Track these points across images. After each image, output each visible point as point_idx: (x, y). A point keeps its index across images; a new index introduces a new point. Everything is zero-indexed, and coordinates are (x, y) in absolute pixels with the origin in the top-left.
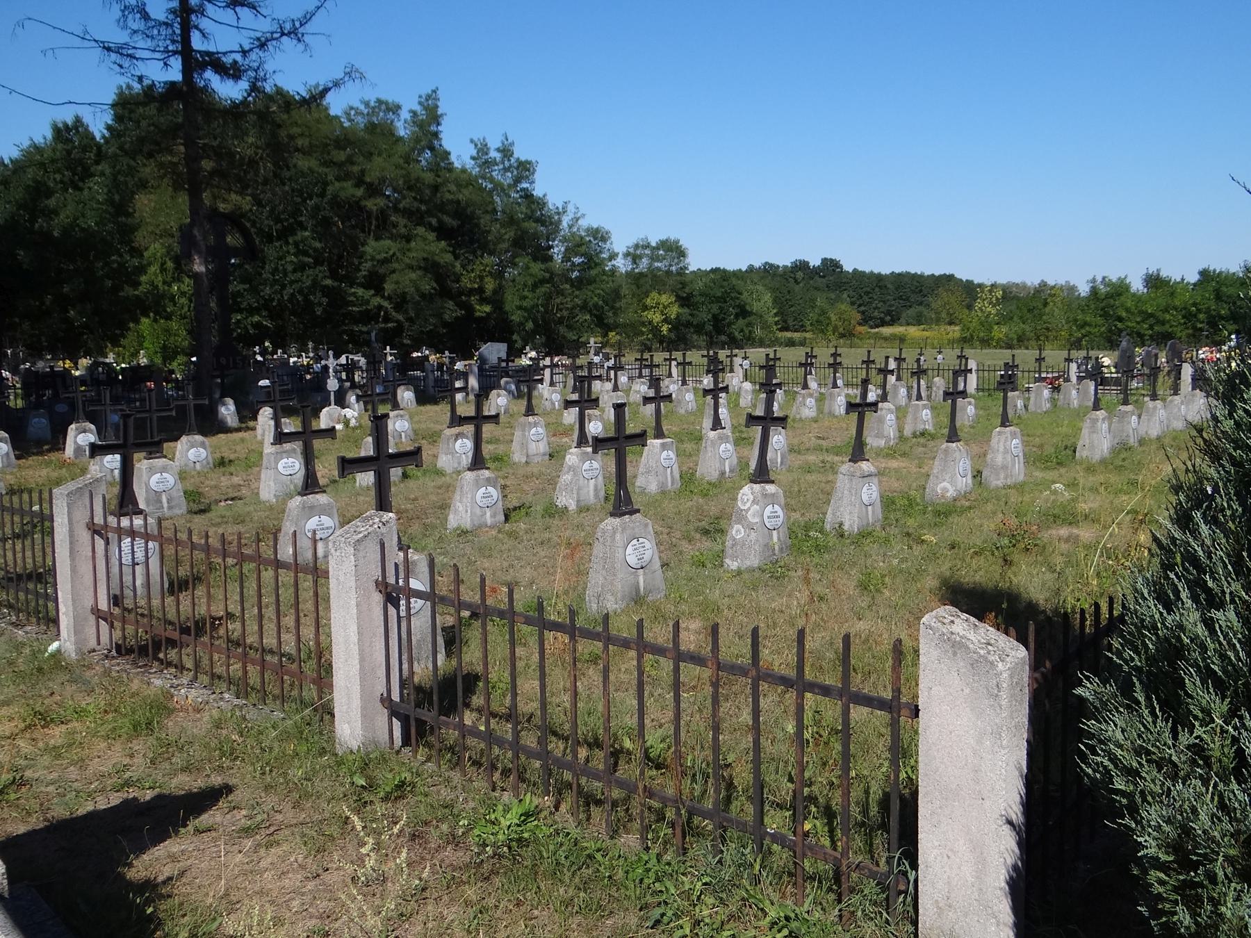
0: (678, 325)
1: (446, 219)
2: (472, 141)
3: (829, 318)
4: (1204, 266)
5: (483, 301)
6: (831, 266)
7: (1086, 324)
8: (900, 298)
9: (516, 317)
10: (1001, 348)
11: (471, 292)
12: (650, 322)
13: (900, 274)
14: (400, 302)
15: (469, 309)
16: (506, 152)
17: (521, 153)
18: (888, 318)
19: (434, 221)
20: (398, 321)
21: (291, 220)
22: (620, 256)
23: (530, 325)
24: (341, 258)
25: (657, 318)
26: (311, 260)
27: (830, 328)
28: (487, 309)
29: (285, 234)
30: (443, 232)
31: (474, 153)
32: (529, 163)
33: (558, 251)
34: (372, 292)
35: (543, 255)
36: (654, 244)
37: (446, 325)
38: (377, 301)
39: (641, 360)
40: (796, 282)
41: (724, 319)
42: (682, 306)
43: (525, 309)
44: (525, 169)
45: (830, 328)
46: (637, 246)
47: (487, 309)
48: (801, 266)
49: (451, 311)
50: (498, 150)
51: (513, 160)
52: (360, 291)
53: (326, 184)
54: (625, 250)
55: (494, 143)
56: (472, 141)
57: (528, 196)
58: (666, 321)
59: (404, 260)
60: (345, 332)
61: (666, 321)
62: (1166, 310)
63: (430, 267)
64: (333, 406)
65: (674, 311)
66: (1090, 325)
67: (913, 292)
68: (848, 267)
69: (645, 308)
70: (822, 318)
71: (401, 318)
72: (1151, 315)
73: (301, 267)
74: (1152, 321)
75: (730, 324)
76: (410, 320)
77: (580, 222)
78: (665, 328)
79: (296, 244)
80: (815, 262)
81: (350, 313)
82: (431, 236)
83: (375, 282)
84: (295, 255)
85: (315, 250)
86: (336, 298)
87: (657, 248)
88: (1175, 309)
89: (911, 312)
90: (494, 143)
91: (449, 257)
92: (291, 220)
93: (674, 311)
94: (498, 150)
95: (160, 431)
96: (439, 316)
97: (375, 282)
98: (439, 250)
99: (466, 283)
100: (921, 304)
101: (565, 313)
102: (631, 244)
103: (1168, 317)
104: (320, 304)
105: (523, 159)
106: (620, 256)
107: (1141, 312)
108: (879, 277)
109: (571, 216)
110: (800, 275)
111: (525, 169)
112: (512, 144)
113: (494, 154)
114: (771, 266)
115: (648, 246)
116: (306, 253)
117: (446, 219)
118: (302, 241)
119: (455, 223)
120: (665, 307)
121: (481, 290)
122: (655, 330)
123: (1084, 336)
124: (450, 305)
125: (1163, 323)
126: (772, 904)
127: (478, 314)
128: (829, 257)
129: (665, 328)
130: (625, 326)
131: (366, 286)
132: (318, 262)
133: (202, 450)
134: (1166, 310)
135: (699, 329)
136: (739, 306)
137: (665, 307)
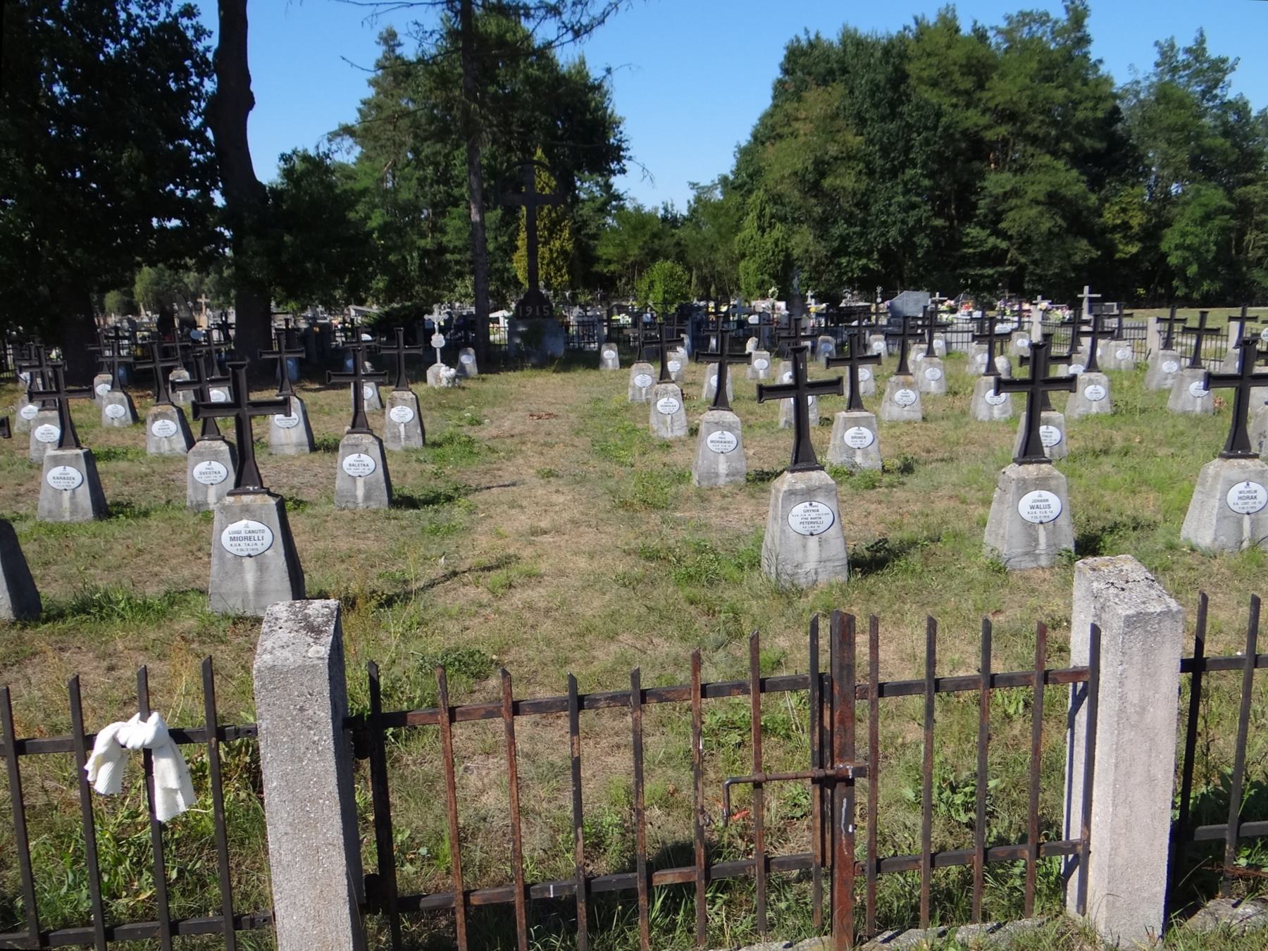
1: (1088, 143)
5: (1129, 239)
11: (1115, 228)
14: (1025, 243)
15: (1110, 249)
17: (1213, 52)
19: (1067, 146)
23: (1193, 270)
24: (959, 200)
29: (894, 173)
30: (1079, 159)
31: (1157, 58)
43: (1188, 248)
44: (1217, 70)
47: (1134, 249)
49: (1083, 250)
50: (1188, 51)
53: (939, 115)
55: (1185, 40)
56: (1157, 44)
59: (1026, 190)
60: (961, 276)
63: (1054, 200)
64: (439, 363)
81: (964, 256)
83: (993, 222)
84: (904, 194)
95: (67, 383)
97: (993, 222)
98: (1071, 181)
99: (1110, 216)
111: (1217, 70)
119: (1100, 146)
121: (1126, 226)
123: (1192, 233)
124: (1084, 243)
133: (120, 407)
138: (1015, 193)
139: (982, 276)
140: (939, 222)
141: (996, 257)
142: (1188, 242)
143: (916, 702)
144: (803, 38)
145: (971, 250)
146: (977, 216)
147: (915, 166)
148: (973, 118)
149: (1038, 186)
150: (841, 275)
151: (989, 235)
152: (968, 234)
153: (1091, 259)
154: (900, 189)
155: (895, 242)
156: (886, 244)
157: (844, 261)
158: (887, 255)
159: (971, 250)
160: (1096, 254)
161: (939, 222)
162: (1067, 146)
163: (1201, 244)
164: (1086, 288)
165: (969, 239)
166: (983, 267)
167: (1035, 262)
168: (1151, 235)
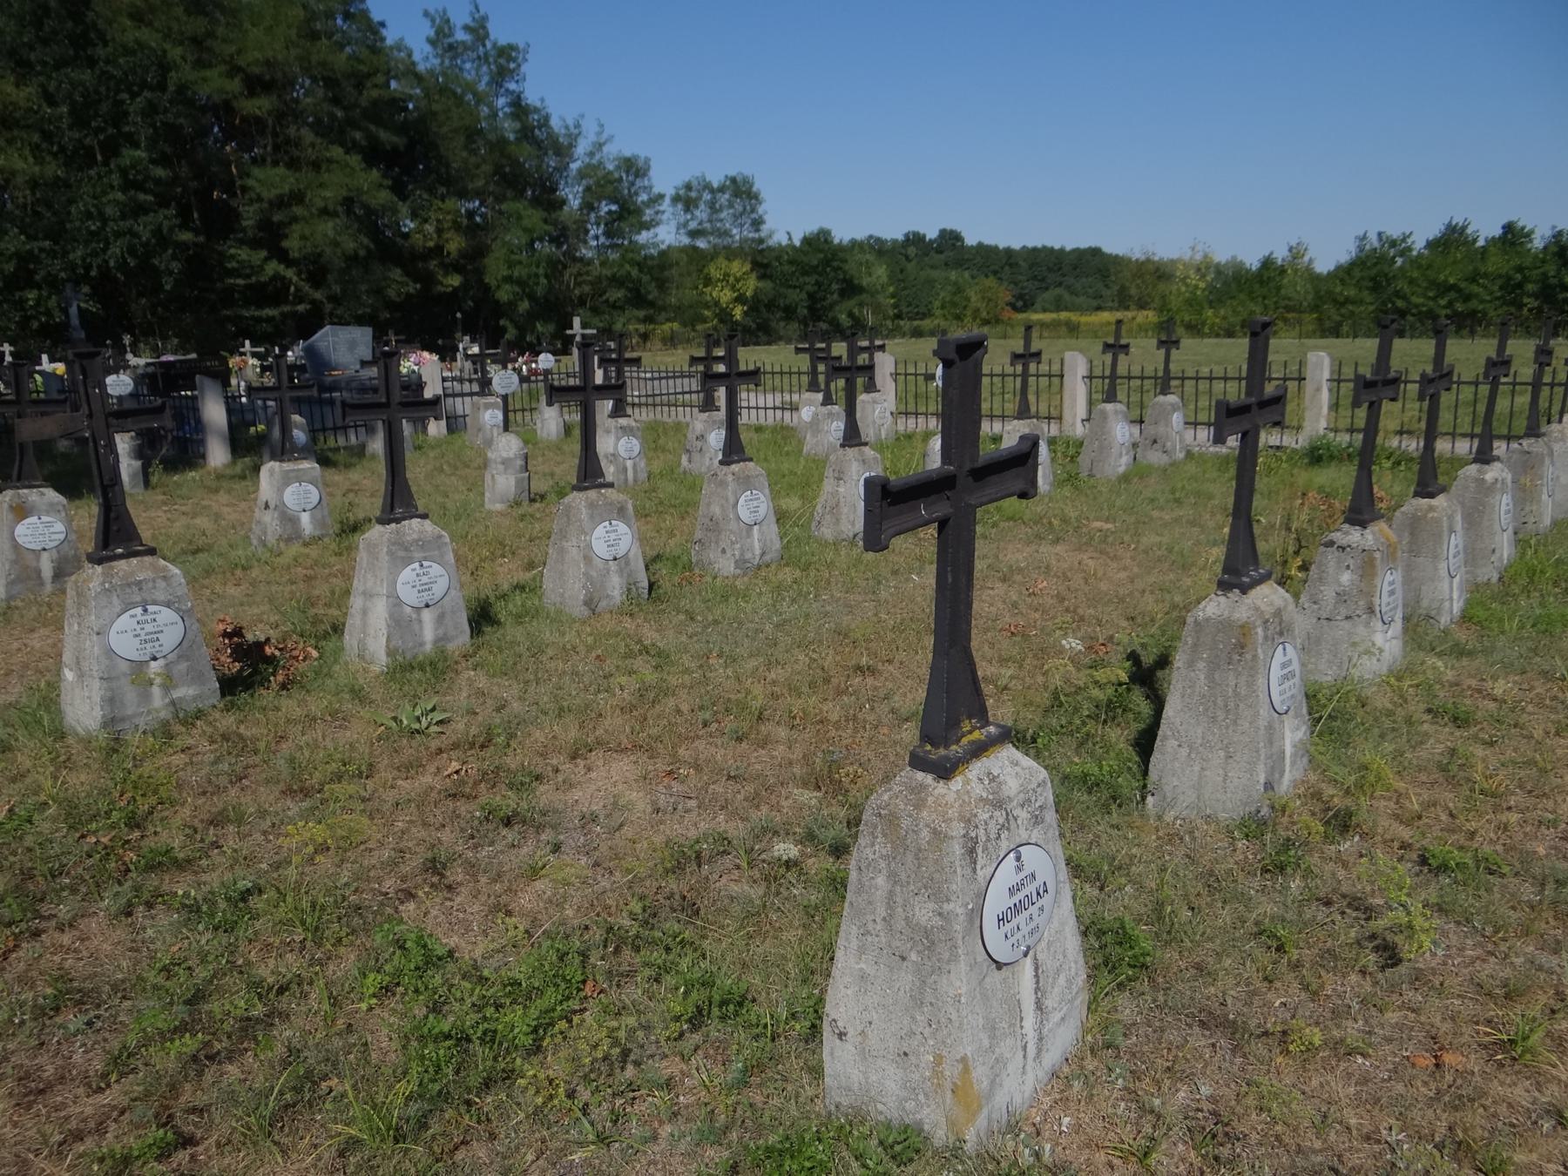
0: (754, 305)
1: (384, 135)
2: (426, 14)
3: (968, 299)
4: (1458, 220)
6: (950, 239)
7: (1347, 301)
8: (1035, 278)
9: (504, 294)
10: (1218, 336)
12: (717, 303)
13: (1035, 249)
15: (428, 280)
16: (479, 30)
17: (500, 34)
18: (1020, 304)
20: (313, 302)
21: (110, 131)
22: (667, 200)
25: (726, 296)
26: (150, 198)
27: (969, 313)
28: (455, 281)
30: (374, 155)
31: (432, 33)
32: (512, 47)
33: (573, 196)
34: (264, 254)
35: (548, 200)
36: (715, 185)
37: (390, 305)
38: (273, 267)
39: (709, 360)
40: (907, 258)
41: (824, 299)
42: (762, 277)
43: (520, 282)
44: (505, 62)
45: (969, 313)
46: (688, 187)
47: (455, 281)
48: (915, 239)
50: (466, 28)
51: (489, 45)
52: (244, 254)
54: (673, 192)
55: (460, 17)
56: (426, 14)
57: (519, 108)
58: (740, 299)
61: (740, 299)
62: (1473, 279)
65: (751, 285)
66: (1353, 303)
67: (1050, 270)
68: (970, 240)
69: (708, 281)
70: (956, 299)
71: (318, 295)
72: (1453, 287)
73: (139, 210)
74: (1453, 295)
75: (832, 306)
76: (332, 299)
77: (605, 149)
78: (738, 312)
79: (124, 172)
80: (932, 234)
82: (355, 160)
83: (270, 237)
85: (158, 181)
86: (201, 266)
87: (722, 189)
88: (1486, 276)
89: (1048, 295)
90: (460, 17)
91: (384, 196)
92: (110, 131)
93: (751, 285)
94: (466, 28)
96: (378, 292)
98: (370, 183)
100: (1060, 284)
101: (587, 289)
102: (680, 183)
103: (1475, 289)
104: (171, 273)
105: (503, 41)
106: (667, 200)
107: (1433, 283)
108: (1009, 252)
109: (592, 138)
110: (912, 251)
112: (484, 19)
113: (461, 36)
114: (878, 240)
115: (707, 186)
116: (138, 186)
117: (384, 135)
118: (133, 166)
119: (399, 141)
120: (738, 280)
122: (724, 316)
124: (396, 274)
125: (1467, 298)
126: (872, 671)
127: (440, 289)
128: (949, 227)
129: (738, 312)
130: (679, 309)
131: (255, 244)
132: (163, 202)
134: (1473, 279)
135: (789, 313)
136: (844, 280)
137: (738, 280)
138: (297, 197)
139: (259, 320)
140: (186, 236)
141: (274, 292)
142: (516, 274)
143: (1459, 431)
144: (1373, 237)
145: (240, 282)
146: (244, 230)
147: (136, 146)
148: (214, 84)
149: (330, 192)
150: (26, 320)
151: (266, 259)
152: (233, 257)
153: (408, 295)
154: (116, 179)
155: (123, 265)
156: (105, 272)
157: (31, 295)
158: (104, 286)
159: (240, 282)
160: (413, 288)
161: (186, 236)
162: (358, 135)
163: (529, 277)
164: (247, 342)
165: (234, 264)
166: (260, 306)
167: (332, 299)
168: (474, 256)
